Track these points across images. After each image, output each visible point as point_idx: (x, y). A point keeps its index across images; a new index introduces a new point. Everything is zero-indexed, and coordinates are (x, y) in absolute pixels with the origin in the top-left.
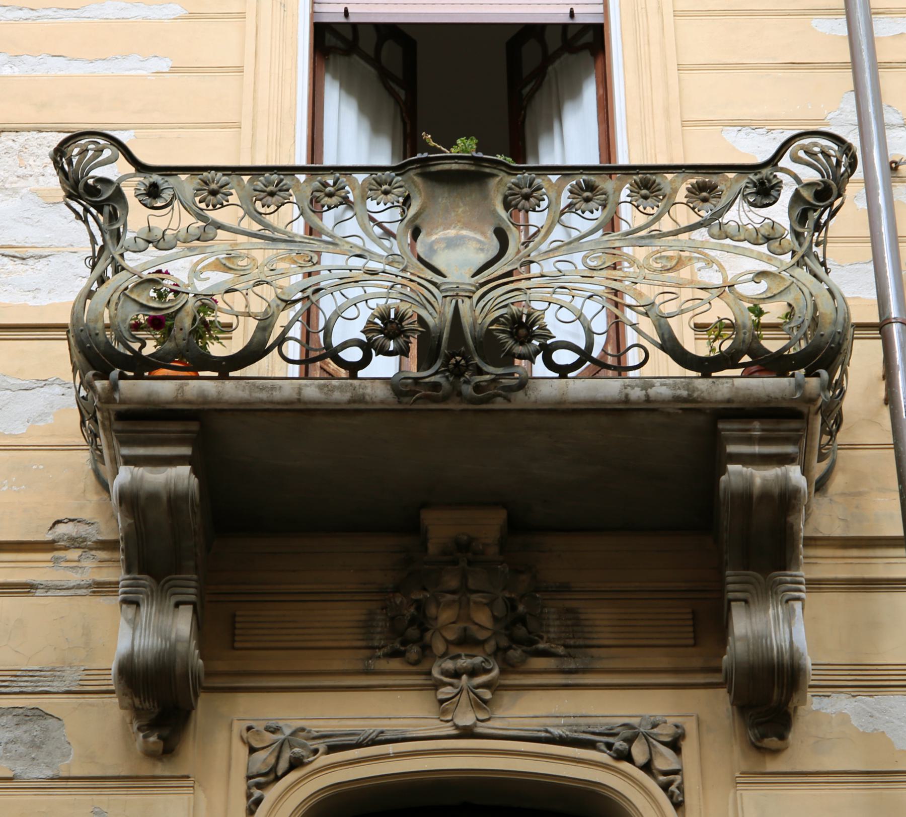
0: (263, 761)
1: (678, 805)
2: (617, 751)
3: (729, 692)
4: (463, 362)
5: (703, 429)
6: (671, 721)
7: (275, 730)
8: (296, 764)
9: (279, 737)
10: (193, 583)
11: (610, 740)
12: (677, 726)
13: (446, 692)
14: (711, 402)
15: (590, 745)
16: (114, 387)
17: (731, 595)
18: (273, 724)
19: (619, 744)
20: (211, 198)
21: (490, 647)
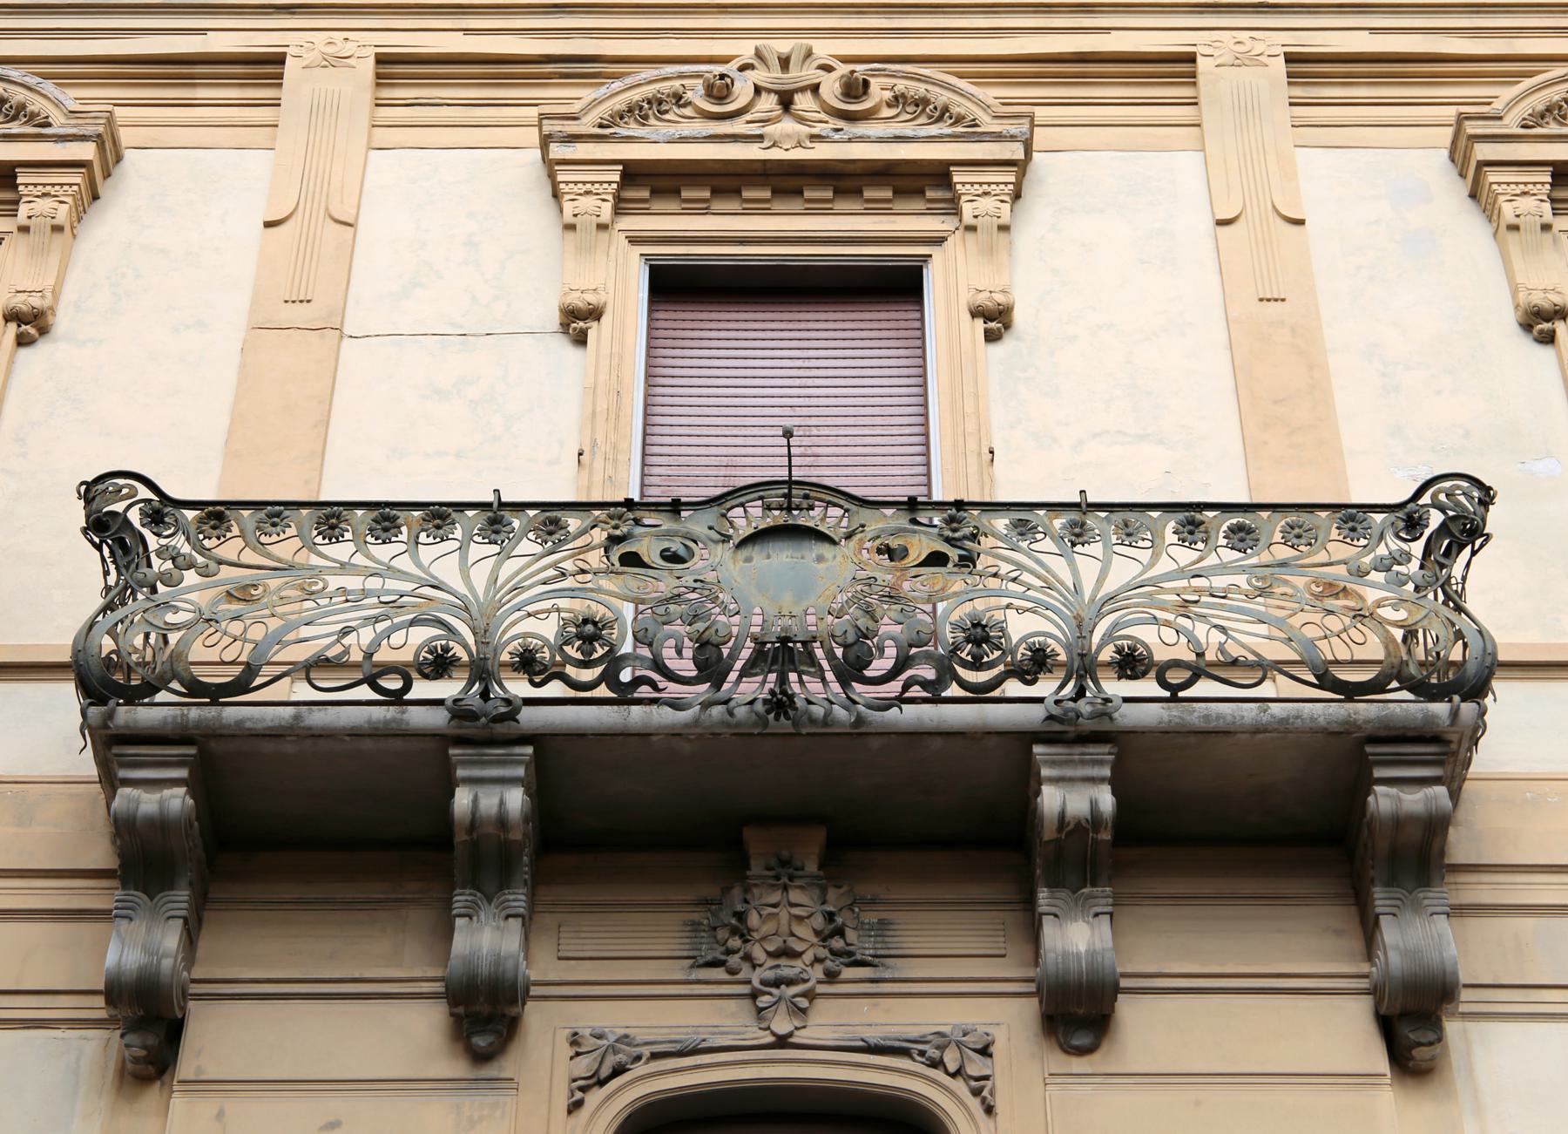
0: (584, 1066)
1: (989, 1110)
3: (1041, 1002)
5: (1354, 756)
6: (981, 1029)
7: (600, 1037)
14: (1266, 731)
15: (903, 1052)
16: (111, 715)
18: (597, 1031)
19: (933, 1053)
21: (808, 957)
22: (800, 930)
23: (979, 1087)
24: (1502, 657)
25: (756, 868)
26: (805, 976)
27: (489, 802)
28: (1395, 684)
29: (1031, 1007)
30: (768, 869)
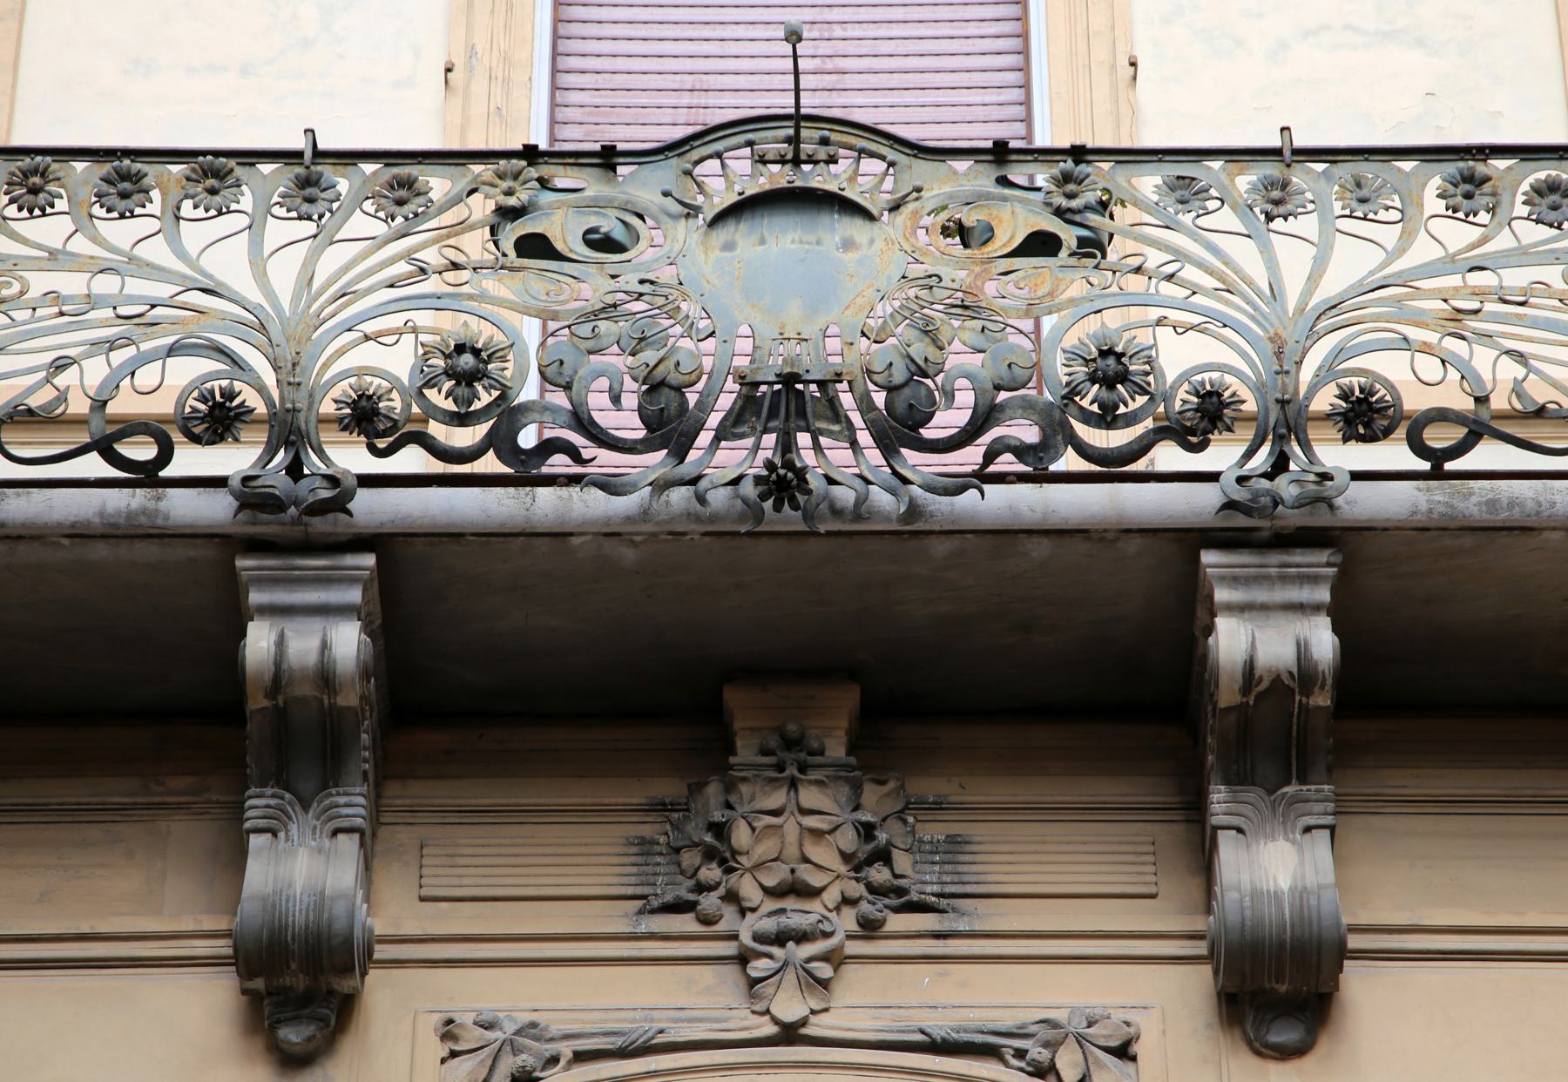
2: (1032, 1063)
3: (1216, 972)
4: (790, 475)
6: (1118, 1016)
7: (489, 1026)
10: (361, 800)
11: (1018, 1043)
17: (1215, 820)
18: (486, 1017)
20: (31, 197)
21: (832, 896)
22: (817, 853)
25: (745, 752)
26: (827, 927)
29: (1198, 983)
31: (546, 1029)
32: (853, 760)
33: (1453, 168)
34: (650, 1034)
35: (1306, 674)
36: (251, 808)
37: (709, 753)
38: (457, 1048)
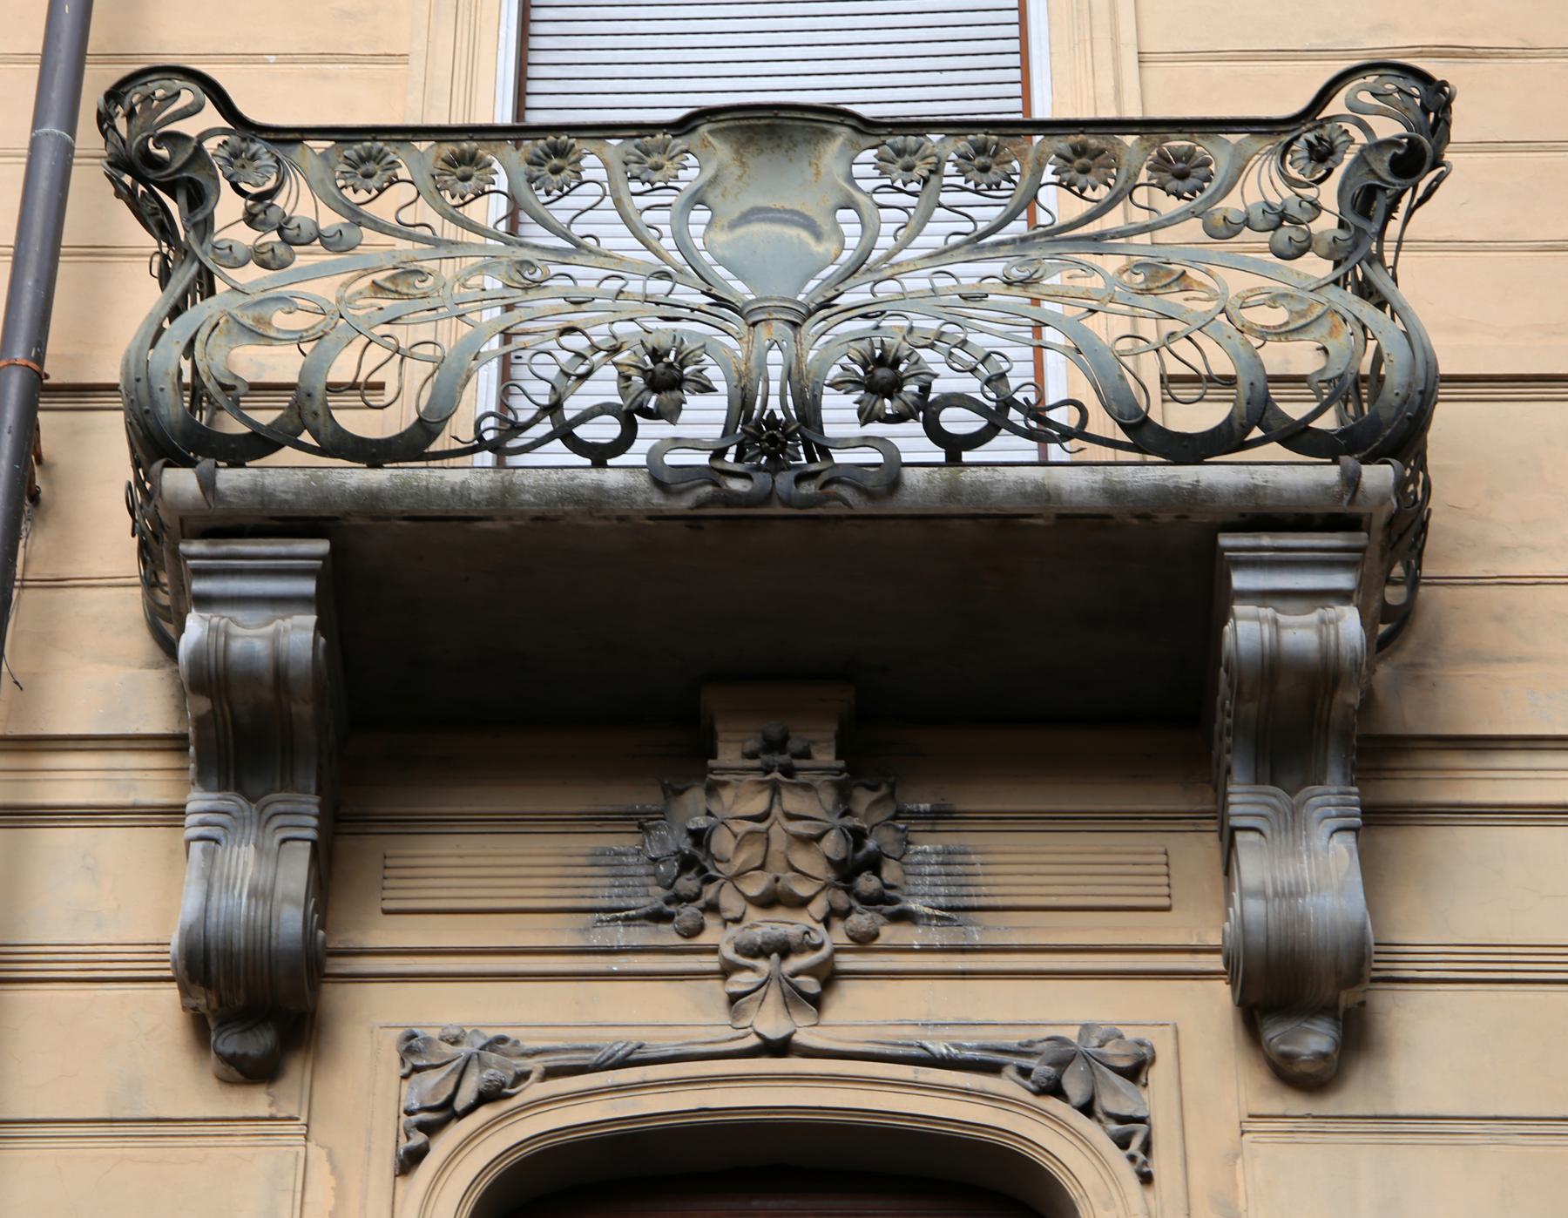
0: (431, 1087)
6: (1130, 1034)
7: (455, 1042)
8: (489, 1095)
9: (464, 1050)
11: (1025, 1062)
12: (1141, 1044)
13: (741, 982)
15: (993, 1069)
17: (1235, 822)
21: (818, 907)
22: (802, 859)
23: (1131, 1133)
24: (1444, 370)
25: (728, 755)
26: (816, 940)
27: (1300, 632)
28: (1257, 433)
29: (1221, 995)
30: (752, 755)
31: (517, 1043)
32: (841, 764)
33: (1063, 144)
34: (628, 1048)
35: (280, 671)
36: (917, 853)
37: (686, 757)
38: (419, 1063)
